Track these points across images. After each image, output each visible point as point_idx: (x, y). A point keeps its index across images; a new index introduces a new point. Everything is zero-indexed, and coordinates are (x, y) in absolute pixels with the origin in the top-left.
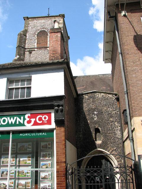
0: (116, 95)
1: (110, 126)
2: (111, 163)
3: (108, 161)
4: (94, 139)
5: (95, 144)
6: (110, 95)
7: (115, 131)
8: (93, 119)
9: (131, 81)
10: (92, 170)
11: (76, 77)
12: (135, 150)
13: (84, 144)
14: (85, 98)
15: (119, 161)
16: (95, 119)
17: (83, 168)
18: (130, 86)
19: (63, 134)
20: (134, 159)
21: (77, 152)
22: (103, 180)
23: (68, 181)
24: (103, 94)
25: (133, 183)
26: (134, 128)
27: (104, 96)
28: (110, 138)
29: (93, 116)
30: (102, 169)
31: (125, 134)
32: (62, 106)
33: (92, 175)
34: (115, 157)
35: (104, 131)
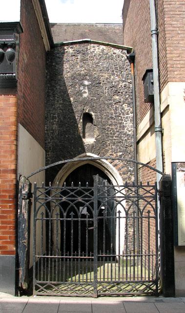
0: (129, 51)
1: (113, 111)
2: (109, 181)
3: (105, 177)
4: (81, 135)
5: (81, 144)
6: (118, 50)
7: (122, 120)
8: (81, 95)
9: (170, 5)
10: (72, 190)
11: (53, 25)
12: (166, 154)
13: (60, 142)
14: (67, 52)
15: (126, 178)
16: (85, 95)
17: (59, 183)
18: (166, 16)
19: (13, 109)
20: (162, 171)
21: (46, 158)
22: (95, 212)
23: (19, 211)
24: (104, 47)
25: (156, 218)
26: (168, 106)
27: (105, 51)
28: (111, 134)
29: (81, 88)
30: (93, 189)
31: (144, 125)
32: (13, 46)
33: (72, 201)
34: (119, 170)
35: (102, 119)
